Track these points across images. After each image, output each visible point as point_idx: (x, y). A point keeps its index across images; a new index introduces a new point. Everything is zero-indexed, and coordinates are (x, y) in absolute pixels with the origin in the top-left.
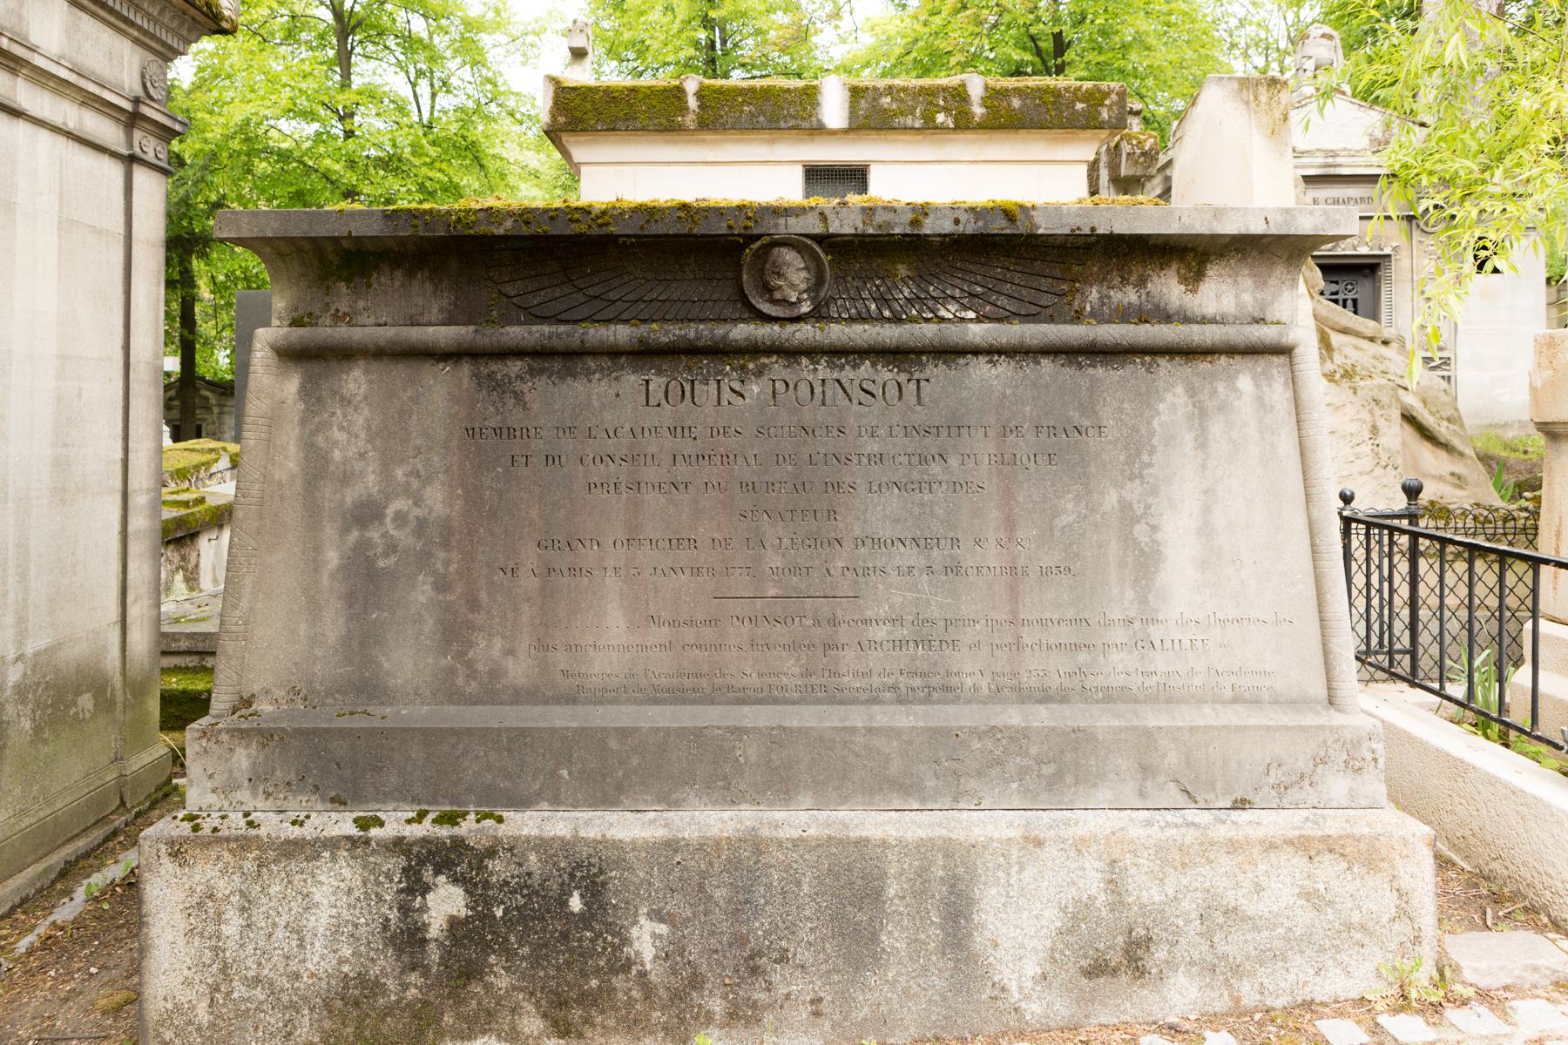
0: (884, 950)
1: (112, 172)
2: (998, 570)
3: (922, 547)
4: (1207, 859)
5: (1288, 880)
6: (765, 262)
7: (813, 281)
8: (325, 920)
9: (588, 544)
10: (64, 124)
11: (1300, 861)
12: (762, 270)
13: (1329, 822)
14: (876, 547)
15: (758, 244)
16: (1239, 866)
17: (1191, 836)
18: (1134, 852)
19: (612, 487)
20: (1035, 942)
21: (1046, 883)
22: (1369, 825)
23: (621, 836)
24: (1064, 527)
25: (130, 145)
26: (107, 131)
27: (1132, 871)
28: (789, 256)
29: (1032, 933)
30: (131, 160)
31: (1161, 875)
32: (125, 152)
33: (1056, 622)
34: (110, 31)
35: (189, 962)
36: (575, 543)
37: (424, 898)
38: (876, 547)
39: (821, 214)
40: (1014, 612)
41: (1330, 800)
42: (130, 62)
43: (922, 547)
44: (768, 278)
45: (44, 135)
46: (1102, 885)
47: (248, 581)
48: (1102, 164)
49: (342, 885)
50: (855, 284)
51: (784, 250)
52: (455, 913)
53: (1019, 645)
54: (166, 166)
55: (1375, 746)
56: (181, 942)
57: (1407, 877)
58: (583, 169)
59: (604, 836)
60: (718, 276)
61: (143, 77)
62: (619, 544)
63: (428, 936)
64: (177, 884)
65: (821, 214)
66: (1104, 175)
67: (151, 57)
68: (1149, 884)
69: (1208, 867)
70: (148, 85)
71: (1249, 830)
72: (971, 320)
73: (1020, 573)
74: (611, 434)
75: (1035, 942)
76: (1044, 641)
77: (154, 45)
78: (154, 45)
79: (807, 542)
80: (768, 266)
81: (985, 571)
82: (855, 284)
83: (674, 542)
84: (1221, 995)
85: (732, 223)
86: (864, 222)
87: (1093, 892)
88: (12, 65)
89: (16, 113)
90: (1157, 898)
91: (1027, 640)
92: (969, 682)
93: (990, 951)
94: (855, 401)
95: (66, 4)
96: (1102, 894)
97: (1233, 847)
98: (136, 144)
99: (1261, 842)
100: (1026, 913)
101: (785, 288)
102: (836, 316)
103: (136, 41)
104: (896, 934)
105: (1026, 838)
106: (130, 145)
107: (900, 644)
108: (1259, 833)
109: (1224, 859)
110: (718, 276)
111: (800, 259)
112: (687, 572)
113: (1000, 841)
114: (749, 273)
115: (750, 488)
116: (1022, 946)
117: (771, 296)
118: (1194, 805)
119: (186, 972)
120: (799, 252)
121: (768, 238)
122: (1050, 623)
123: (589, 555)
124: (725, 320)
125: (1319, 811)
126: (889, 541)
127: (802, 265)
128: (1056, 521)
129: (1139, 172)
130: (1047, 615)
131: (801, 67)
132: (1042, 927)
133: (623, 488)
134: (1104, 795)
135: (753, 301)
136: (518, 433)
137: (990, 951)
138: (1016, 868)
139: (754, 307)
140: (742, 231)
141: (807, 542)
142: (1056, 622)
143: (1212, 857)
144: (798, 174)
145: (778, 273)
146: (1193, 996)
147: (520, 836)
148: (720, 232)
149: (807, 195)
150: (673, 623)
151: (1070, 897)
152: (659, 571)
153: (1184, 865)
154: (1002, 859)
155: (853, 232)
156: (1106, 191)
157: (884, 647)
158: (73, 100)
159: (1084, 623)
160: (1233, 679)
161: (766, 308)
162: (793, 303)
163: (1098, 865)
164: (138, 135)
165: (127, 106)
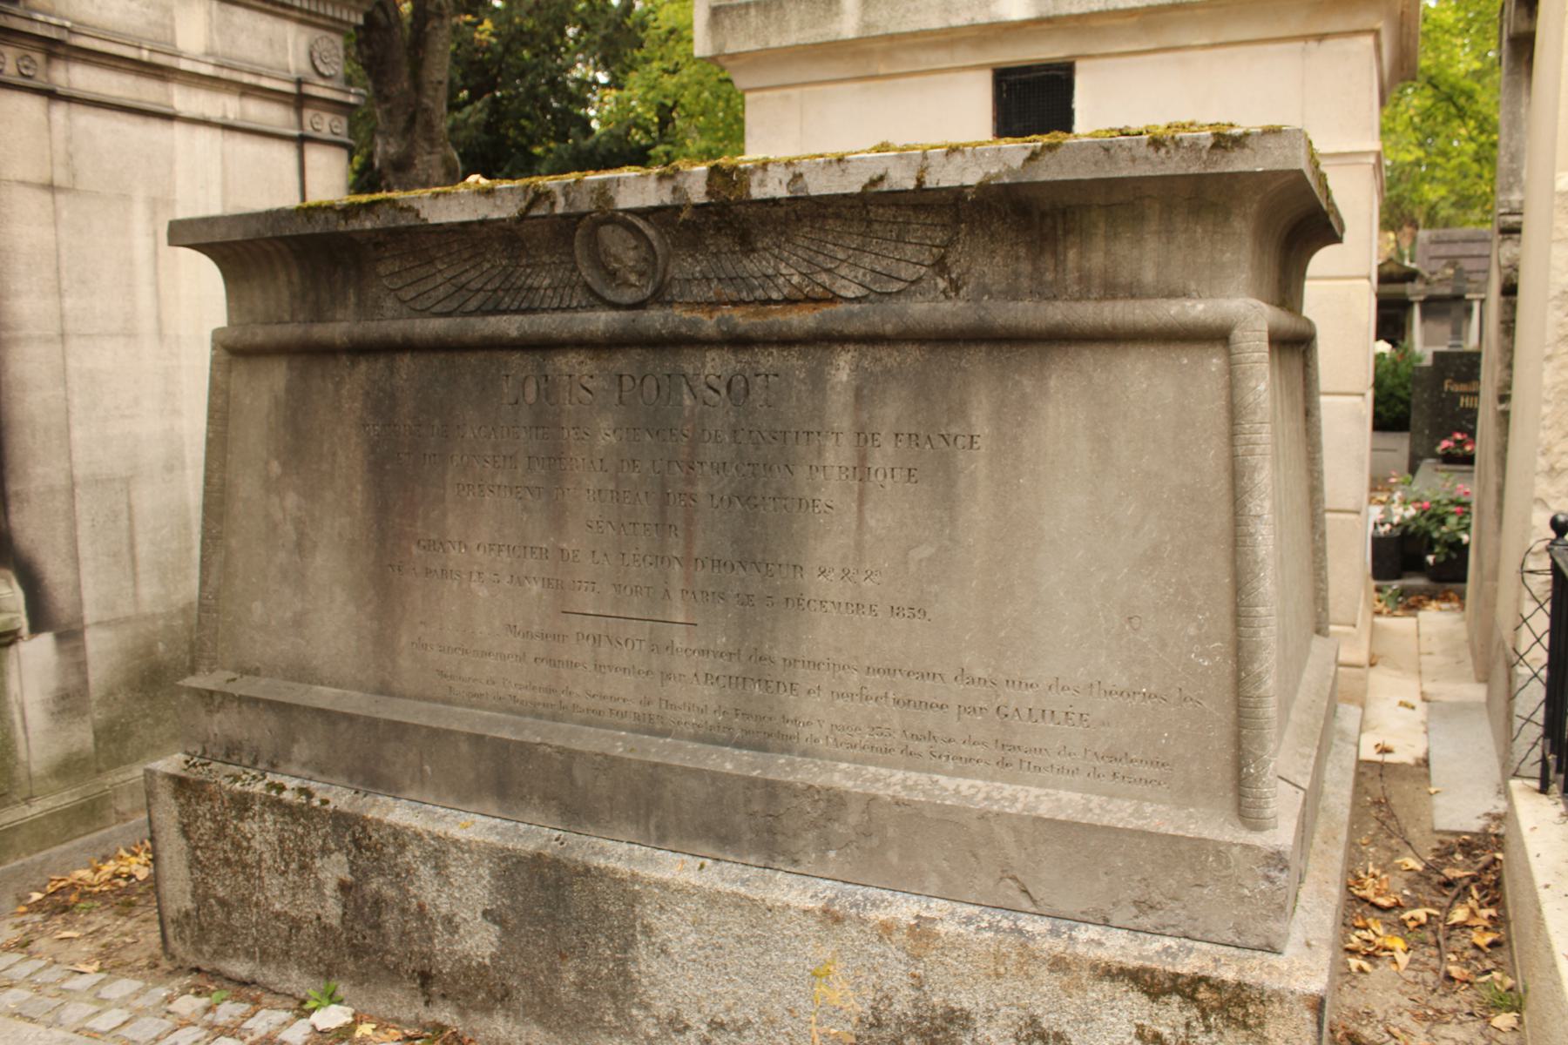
1: (285, 155)
4: (1026, 974)
10: (225, 117)
16: (1063, 988)
24: (921, 560)
25: (301, 125)
26: (275, 116)
29: (830, 1012)
30: (302, 141)
32: (296, 133)
34: (269, 18)
41: (1208, 931)
42: (296, 45)
45: (203, 134)
46: (905, 978)
54: (346, 140)
58: (749, 97)
61: (311, 55)
67: (319, 33)
68: (957, 987)
69: (1027, 982)
70: (318, 62)
77: (321, 21)
78: (321, 21)
88: (159, 73)
89: (170, 117)
92: (806, 732)
95: (215, 5)
97: (1058, 964)
98: (306, 121)
99: (1094, 967)
103: (301, 22)
105: (825, 911)
106: (301, 125)
108: (1095, 953)
109: (1043, 973)
118: (1033, 909)
128: (912, 553)
143: (1031, 973)
158: (232, 93)
159: (938, 677)
163: (902, 956)
164: (308, 114)
165: (289, 88)
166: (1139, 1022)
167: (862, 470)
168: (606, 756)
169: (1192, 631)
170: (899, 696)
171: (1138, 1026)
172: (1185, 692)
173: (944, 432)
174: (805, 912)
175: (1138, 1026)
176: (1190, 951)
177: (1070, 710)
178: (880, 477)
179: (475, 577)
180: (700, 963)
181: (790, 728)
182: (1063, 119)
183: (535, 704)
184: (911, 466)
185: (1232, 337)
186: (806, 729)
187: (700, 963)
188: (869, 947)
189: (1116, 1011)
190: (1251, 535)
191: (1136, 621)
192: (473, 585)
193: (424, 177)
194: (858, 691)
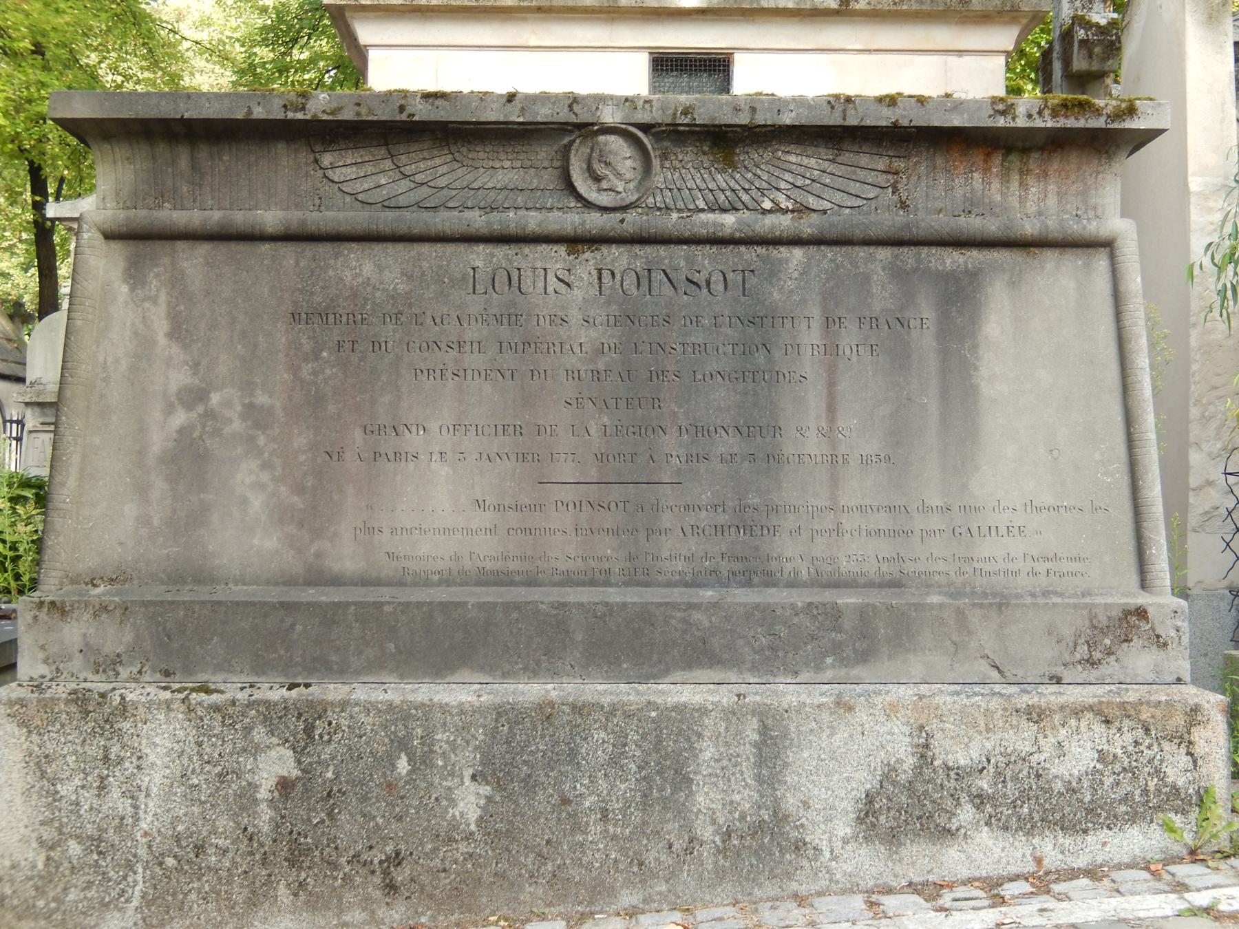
0: (700, 810)
2: (819, 458)
3: (745, 434)
5: (1089, 745)
7: (640, 169)
8: (158, 779)
9: (414, 429)
11: (1099, 728)
13: (1130, 693)
14: (700, 435)
17: (995, 703)
18: (940, 718)
19: (438, 372)
20: (845, 804)
21: (856, 747)
22: (1168, 695)
23: (447, 700)
27: (939, 735)
28: (615, 142)
29: (843, 795)
31: (966, 740)
33: (875, 509)
35: (26, 820)
36: (401, 428)
37: (255, 759)
38: (700, 435)
40: (834, 497)
41: (1137, 675)
43: (745, 434)
46: (910, 749)
47: (76, 459)
48: (1055, 55)
49: (176, 747)
51: (612, 138)
52: (286, 774)
53: (838, 531)
55: (1179, 624)
56: (19, 800)
57: (1202, 742)
58: (372, 55)
59: (431, 700)
62: (444, 430)
63: (259, 796)
64: (15, 744)
66: (1057, 67)
69: (1011, 732)
71: (1052, 698)
73: (840, 462)
74: (438, 320)
75: (845, 804)
76: (864, 527)
79: (631, 429)
81: (807, 459)
83: (500, 429)
84: (1024, 855)
87: (902, 755)
90: (962, 762)
91: (847, 526)
92: (788, 567)
93: (801, 813)
94: (681, 292)
96: (910, 757)
100: (837, 776)
101: (611, 177)
104: (712, 795)
107: (720, 529)
112: (513, 458)
113: (812, 706)
115: (576, 375)
116: (833, 808)
118: (1003, 680)
119: (22, 830)
122: (869, 510)
123: (413, 441)
125: (1124, 686)
126: (712, 429)
129: (1095, 66)
130: (868, 502)
132: (853, 789)
133: (449, 374)
134: (917, 669)
136: (344, 319)
137: (801, 813)
138: (828, 732)
141: (631, 429)
142: (875, 509)
144: (642, 62)
146: (996, 856)
147: (349, 699)
149: (654, 88)
150: (498, 508)
151: (879, 760)
152: (484, 457)
153: (988, 730)
154: (814, 723)
156: (1059, 89)
157: (706, 533)
160: (1049, 565)
161: (592, 195)
163: (906, 730)
166: (1100, 748)
167: (831, 350)
168: (607, 604)
169: (1097, 456)
170: (871, 527)
171: (1099, 752)
172: (1096, 504)
173: (899, 316)
174: (819, 706)
175: (1099, 752)
176: (1127, 690)
177: (1009, 524)
178: (848, 352)
179: (436, 457)
180: (717, 776)
181: (774, 565)
182: (725, 86)
183: (508, 573)
184: (873, 343)
185: (1116, 244)
186: (788, 565)
187: (717, 776)
188: (877, 728)
189: (1082, 742)
190: (1140, 382)
191: (1055, 453)
192: (433, 465)
193: (627, 104)
194: (835, 527)
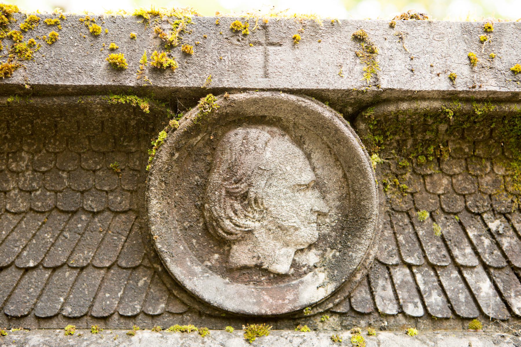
6: (210, 168)
12: (203, 187)
15: (193, 114)
39: (358, 39)
44: (218, 211)
50: (439, 229)
60: (90, 203)
65: (358, 39)
72: (50, 276)
80: (216, 178)
82: (439, 229)
85: (119, 57)
86: (471, 62)
101: (261, 235)
102: (391, 309)
110: (90, 203)
111: (300, 160)
114: (166, 195)
117: (226, 256)
120: (299, 142)
121: (217, 102)
124: (104, 319)
127: (308, 177)
131: (271, 75)
135: (177, 271)
139: (181, 288)
140: (149, 80)
145: (245, 196)
148: (85, 81)
155: (444, 85)
162: (281, 277)
